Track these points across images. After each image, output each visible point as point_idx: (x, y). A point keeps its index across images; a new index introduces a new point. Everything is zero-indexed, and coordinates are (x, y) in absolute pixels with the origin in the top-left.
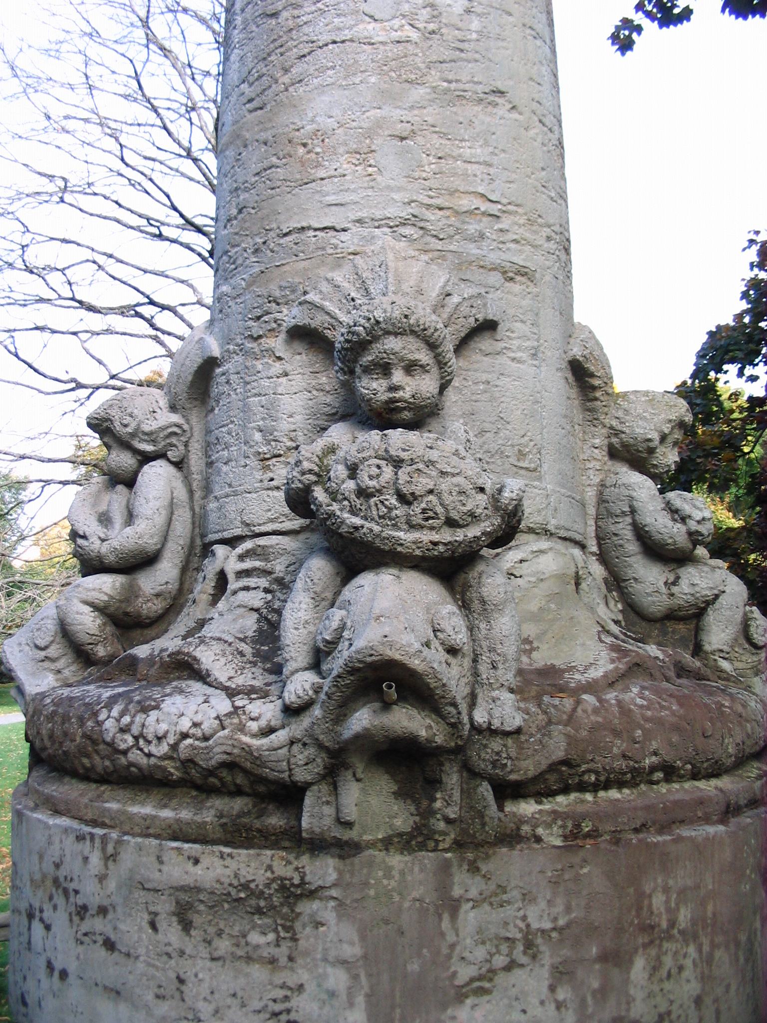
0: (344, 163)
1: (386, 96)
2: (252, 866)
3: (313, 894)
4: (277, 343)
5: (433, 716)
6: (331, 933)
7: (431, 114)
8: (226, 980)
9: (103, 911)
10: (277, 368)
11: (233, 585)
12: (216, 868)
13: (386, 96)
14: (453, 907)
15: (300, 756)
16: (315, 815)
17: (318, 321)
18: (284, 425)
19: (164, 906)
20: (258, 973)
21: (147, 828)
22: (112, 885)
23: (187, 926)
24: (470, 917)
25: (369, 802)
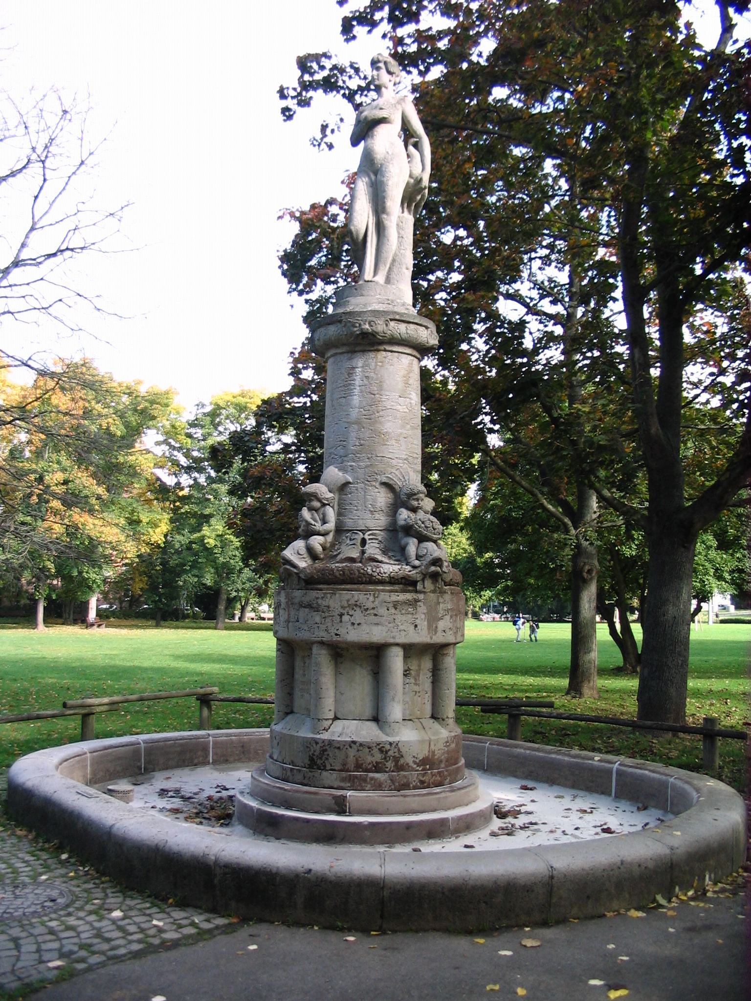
0: (393, 442)
1: (403, 427)
2: (409, 596)
3: (419, 601)
4: (377, 485)
5: (10, 621)
6: (422, 608)
7: (410, 432)
8: (404, 618)
9: (373, 608)
10: (376, 490)
11: (368, 542)
12: (402, 597)
13: (403, 427)
14: (439, 603)
15: (418, 575)
16: (419, 587)
17: (391, 482)
18: (379, 505)
19: (391, 605)
20: (410, 616)
21: (383, 591)
22: (376, 603)
23: (396, 609)
24: (441, 605)
25: (429, 584)
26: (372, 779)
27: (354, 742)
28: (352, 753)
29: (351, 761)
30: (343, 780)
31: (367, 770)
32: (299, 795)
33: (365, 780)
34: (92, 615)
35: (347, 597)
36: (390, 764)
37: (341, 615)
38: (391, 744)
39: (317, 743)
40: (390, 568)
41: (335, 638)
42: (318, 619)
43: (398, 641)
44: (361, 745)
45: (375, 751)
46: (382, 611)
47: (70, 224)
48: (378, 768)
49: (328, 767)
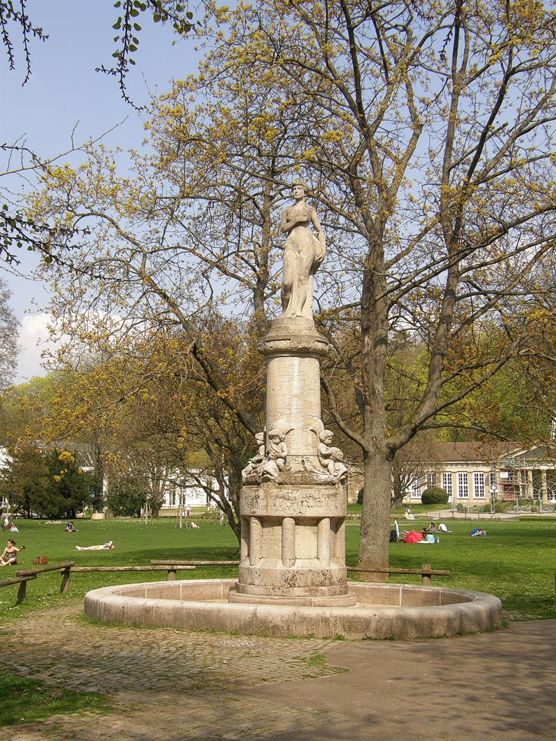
11: (305, 462)
26: (320, 590)
27: (311, 570)
28: (310, 576)
30: (306, 591)
31: (317, 586)
32: (183, 562)
36: (327, 582)
40: (323, 477)
41: (299, 515)
42: (289, 504)
43: (327, 516)
45: (321, 574)
46: (322, 499)
47: (23, 139)
48: (322, 584)
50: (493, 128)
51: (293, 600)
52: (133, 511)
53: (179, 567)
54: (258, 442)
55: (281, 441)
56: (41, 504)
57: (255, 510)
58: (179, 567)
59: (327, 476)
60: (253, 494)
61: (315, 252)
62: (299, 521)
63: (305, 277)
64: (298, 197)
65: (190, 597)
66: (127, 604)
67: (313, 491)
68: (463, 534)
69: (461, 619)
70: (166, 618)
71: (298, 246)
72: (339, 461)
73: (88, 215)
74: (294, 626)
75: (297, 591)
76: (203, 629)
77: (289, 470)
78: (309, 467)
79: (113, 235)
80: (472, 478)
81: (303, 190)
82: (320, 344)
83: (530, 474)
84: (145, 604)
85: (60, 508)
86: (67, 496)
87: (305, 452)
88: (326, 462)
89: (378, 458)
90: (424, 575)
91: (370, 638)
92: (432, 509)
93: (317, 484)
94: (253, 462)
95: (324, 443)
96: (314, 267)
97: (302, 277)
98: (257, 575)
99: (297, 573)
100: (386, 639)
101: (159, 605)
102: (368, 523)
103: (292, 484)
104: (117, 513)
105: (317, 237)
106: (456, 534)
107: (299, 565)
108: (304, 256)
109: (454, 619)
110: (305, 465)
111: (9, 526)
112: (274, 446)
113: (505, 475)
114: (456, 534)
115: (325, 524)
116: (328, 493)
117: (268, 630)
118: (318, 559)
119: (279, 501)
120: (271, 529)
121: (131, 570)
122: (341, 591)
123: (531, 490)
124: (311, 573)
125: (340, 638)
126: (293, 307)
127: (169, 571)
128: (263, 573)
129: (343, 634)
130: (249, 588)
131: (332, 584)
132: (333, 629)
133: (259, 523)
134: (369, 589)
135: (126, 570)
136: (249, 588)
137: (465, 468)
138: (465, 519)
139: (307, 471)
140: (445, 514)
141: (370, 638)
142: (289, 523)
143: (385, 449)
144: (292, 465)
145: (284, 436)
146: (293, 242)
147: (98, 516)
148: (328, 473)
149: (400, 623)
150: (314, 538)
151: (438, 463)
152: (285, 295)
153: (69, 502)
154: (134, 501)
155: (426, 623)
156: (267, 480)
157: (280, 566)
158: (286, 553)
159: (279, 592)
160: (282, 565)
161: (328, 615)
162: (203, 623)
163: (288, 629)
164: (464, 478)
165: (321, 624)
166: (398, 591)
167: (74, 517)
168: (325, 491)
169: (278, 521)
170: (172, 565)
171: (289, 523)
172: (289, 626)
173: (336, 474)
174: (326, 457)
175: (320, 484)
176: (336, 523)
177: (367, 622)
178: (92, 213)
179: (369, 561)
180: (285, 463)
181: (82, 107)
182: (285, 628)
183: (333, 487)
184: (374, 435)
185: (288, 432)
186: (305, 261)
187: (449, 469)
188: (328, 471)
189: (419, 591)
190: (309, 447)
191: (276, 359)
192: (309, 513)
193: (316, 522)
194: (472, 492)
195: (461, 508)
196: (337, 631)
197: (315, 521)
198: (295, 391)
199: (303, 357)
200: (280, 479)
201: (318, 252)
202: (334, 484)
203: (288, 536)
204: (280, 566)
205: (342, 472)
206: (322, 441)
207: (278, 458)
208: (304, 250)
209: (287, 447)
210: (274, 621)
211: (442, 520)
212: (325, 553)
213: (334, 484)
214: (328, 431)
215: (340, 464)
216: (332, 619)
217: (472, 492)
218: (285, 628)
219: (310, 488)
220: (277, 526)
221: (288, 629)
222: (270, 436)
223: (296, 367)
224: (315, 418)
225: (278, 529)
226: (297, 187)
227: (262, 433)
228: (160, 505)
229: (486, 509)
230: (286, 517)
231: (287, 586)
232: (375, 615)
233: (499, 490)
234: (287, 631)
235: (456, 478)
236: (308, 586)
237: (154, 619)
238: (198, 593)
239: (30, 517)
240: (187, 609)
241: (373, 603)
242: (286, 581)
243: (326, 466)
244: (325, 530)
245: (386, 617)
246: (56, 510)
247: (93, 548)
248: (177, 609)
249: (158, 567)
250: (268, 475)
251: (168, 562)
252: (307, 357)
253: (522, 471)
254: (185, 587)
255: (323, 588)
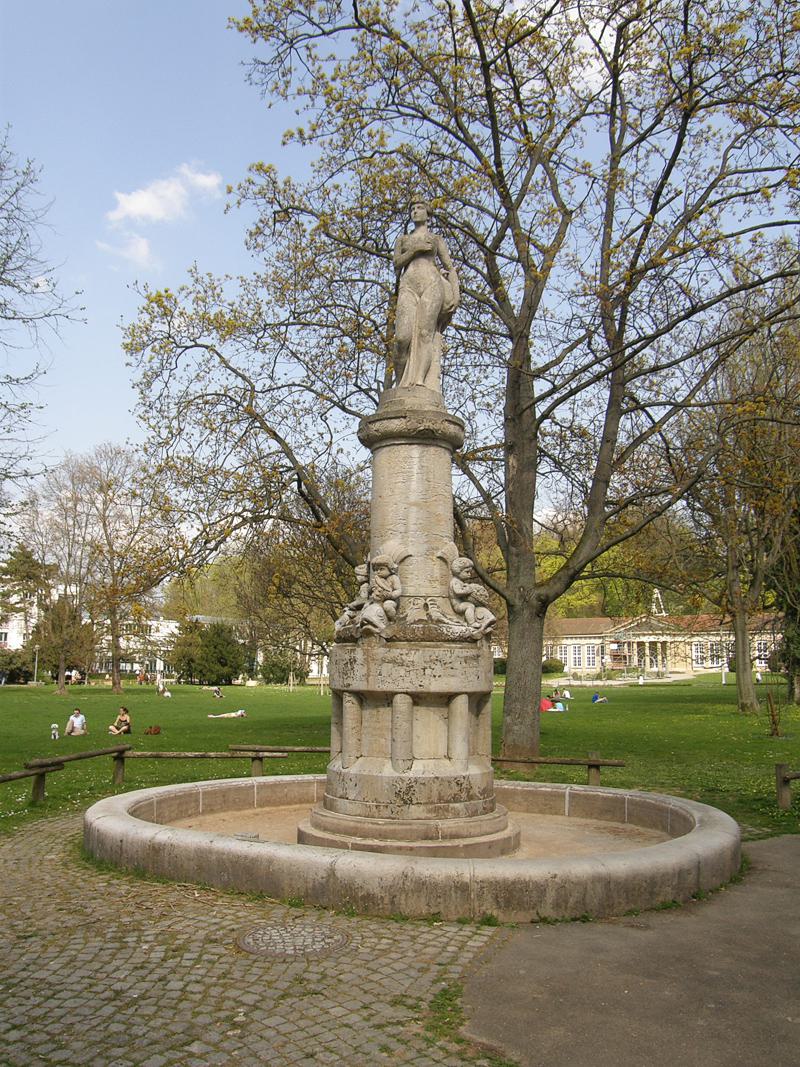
11: (430, 607)
17: (445, 557)
26: (453, 808)
27: (437, 778)
28: (435, 787)
29: (435, 794)
30: (429, 811)
31: (448, 802)
33: (447, 810)
34: (647, 645)
35: (430, 653)
37: (424, 669)
38: (464, 778)
39: (403, 781)
40: (458, 629)
41: (420, 689)
43: (464, 690)
44: (442, 779)
45: (454, 784)
46: (457, 665)
48: (456, 799)
49: (415, 801)
50: (670, 184)
51: (408, 827)
52: (283, 680)
53: (266, 754)
54: (359, 578)
55: (392, 574)
56: (201, 672)
57: (350, 681)
58: (266, 754)
59: (464, 628)
60: (347, 657)
61: (443, 295)
62: (418, 699)
63: (429, 330)
64: (418, 219)
65: (269, 801)
66: (127, 835)
67: (441, 651)
68: (586, 701)
69: (699, 869)
70: (185, 865)
71: (418, 286)
72: (484, 606)
73: (192, 347)
74: (403, 897)
75: (415, 811)
76: (243, 890)
77: (405, 618)
78: (435, 613)
79: (217, 365)
80: (584, 649)
81: (425, 211)
82: (452, 426)
83: (635, 646)
84: (153, 838)
85: (218, 676)
86: (224, 665)
87: (430, 591)
88: (462, 606)
89: (526, 613)
90: (591, 766)
91: (544, 920)
92: (550, 678)
93: (448, 641)
94: (350, 609)
95: (458, 578)
96: (443, 320)
97: (424, 332)
98: (352, 784)
99: (416, 781)
100: (574, 920)
101: (174, 841)
102: (514, 697)
103: (407, 640)
104: (269, 681)
105: (447, 278)
106: (580, 701)
107: (419, 769)
108: (427, 300)
109: (689, 872)
110: (430, 610)
111: (164, 691)
112: (380, 581)
113: (614, 646)
114: (580, 701)
115: (461, 705)
116: (465, 654)
117: (356, 902)
118: (450, 759)
119: (386, 668)
120: (374, 712)
121: (203, 757)
122: (484, 808)
123: (636, 659)
124: (438, 783)
125: (489, 921)
126: (410, 375)
127: (254, 759)
128: (361, 781)
129: (495, 913)
130: (340, 803)
131: (470, 798)
132: (476, 904)
133: (355, 701)
134: (522, 792)
135: (196, 757)
136: (340, 803)
137: (578, 641)
138: (581, 686)
139: (432, 620)
140: (563, 682)
141: (544, 920)
142: (402, 703)
143: (535, 602)
144: (408, 611)
145: (396, 566)
146: (411, 281)
147: (251, 683)
148: (466, 624)
149: (599, 888)
150: (442, 726)
151: (556, 637)
152: (400, 358)
153: (226, 670)
154: (284, 670)
155: (644, 884)
156: (369, 633)
157: (388, 771)
158: (398, 750)
159: (387, 812)
160: (392, 770)
161: (466, 878)
162: (244, 880)
163: (392, 902)
164: (578, 649)
165: (453, 895)
166: (563, 795)
167: (229, 683)
168: (460, 651)
169: (386, 699)
170: (257, 751)
171: (402, 703)
172: (395, 896)
173: (478, 625)
174: (463, 598)
175: (454, 641)
176: (478, 701)
177: (540, 888)
178: (197, 345)
179: (515, 745)
180: (397, 608)
181: (169, 212)
182: (386, 901)
183: (473, 645)
184: (519, 585)
185: (403, 560)
186: (428, 307)
187: (564, 641)
188: (466, 620)
189: (594, 796)
190: (436, 584)
191: (387, 449)
192: (436, 686)
193: (446, 700)
194: (585, 663)
195: (575, 677)
196: (484, 908)
197: (446, 699)
198: (413, 498)
199: (427, 445)
200: (389, 633)
201: (448, 297)
202: (475, 641)
203: (402, 724)
204: (388, 771)
205: (487, 622)
206: (456, 575)
207: (386, 600)
208: (428, 291)
209: (402, 583)
210: (366, 887)
211: (565, 688)
212: (460, 748)
213: (475, 641)
214: (465, 559)
215: (484, 609)
216: (476, 887)
217: (585, 663)
218: (386, 901)
219: (437, 647)
220: (384, 706)
221: (392, 902)
222: (374, 565)
223: (416, 460)
224: (446, 540)
225: (385, 712)
226: (416, 206)
227: (365, 566)
228: (307, 674)
229: (598, 677)
230: (397, 693)
231: (399, 802)
232: (555, 876)
233: (608, 659)
234: (390, 907)
235: (570, 650)
236: (432, 803)
237: (166, 865)
238: (280, 795)
239: (193, 683)
240: (217, 852)
241: (527, 811)
242: (397, 794)
243: (461, 614)
244: (461, 712)
245: (574, 880)
246: (214, 678)
247: (225, 715)
248: (202, 852)
249: (238, 754)
250: (370, 627)
251: (251, 747)
252: (433, 445)
253: (629, 643)
254: (262, 787)
255: (457, 805)
